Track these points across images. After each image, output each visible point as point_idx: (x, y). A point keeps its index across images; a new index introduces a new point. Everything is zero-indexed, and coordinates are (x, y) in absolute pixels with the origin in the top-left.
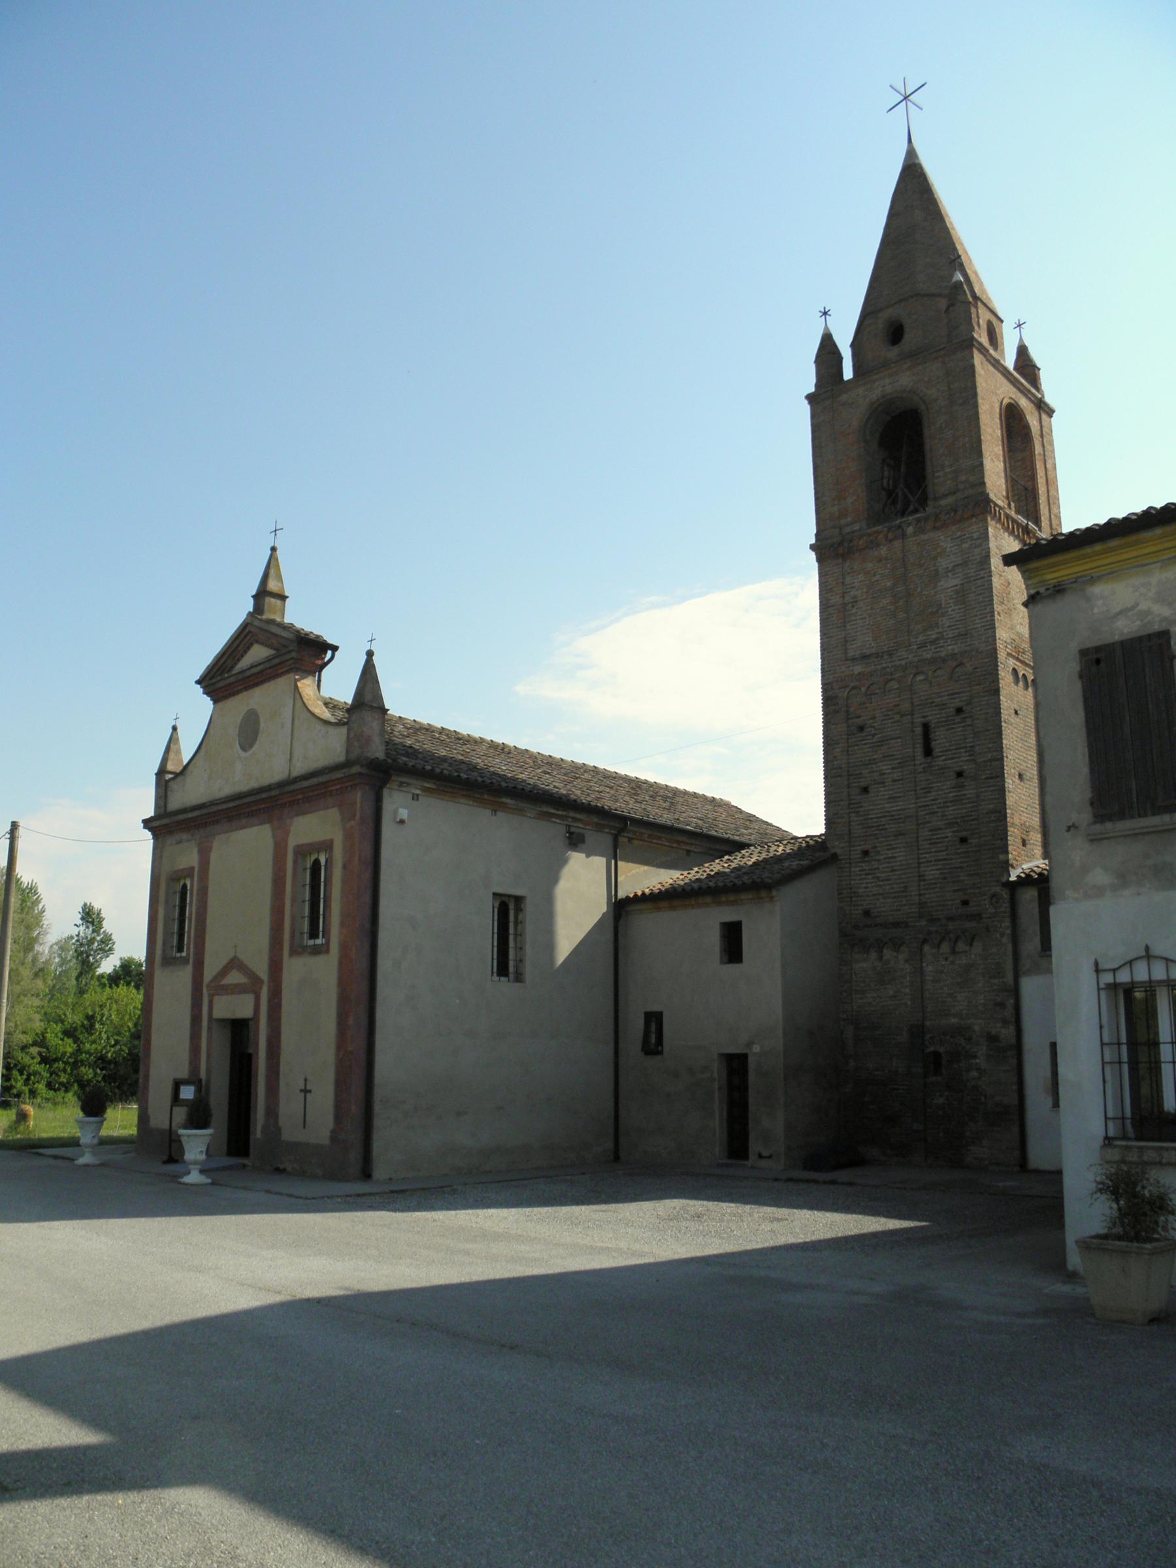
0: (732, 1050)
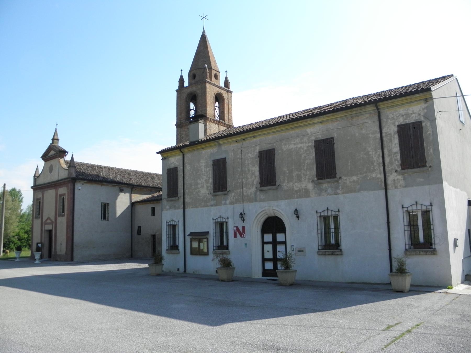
0: (153, 234)
